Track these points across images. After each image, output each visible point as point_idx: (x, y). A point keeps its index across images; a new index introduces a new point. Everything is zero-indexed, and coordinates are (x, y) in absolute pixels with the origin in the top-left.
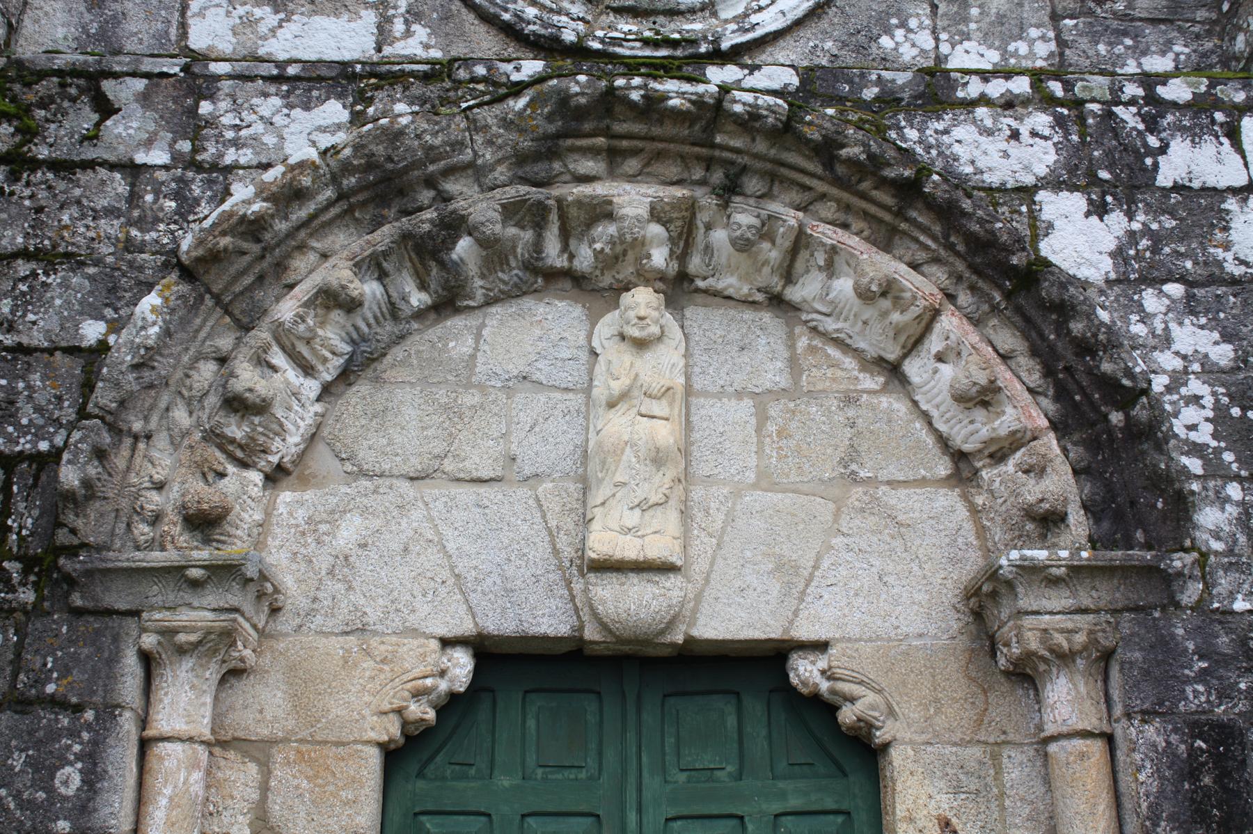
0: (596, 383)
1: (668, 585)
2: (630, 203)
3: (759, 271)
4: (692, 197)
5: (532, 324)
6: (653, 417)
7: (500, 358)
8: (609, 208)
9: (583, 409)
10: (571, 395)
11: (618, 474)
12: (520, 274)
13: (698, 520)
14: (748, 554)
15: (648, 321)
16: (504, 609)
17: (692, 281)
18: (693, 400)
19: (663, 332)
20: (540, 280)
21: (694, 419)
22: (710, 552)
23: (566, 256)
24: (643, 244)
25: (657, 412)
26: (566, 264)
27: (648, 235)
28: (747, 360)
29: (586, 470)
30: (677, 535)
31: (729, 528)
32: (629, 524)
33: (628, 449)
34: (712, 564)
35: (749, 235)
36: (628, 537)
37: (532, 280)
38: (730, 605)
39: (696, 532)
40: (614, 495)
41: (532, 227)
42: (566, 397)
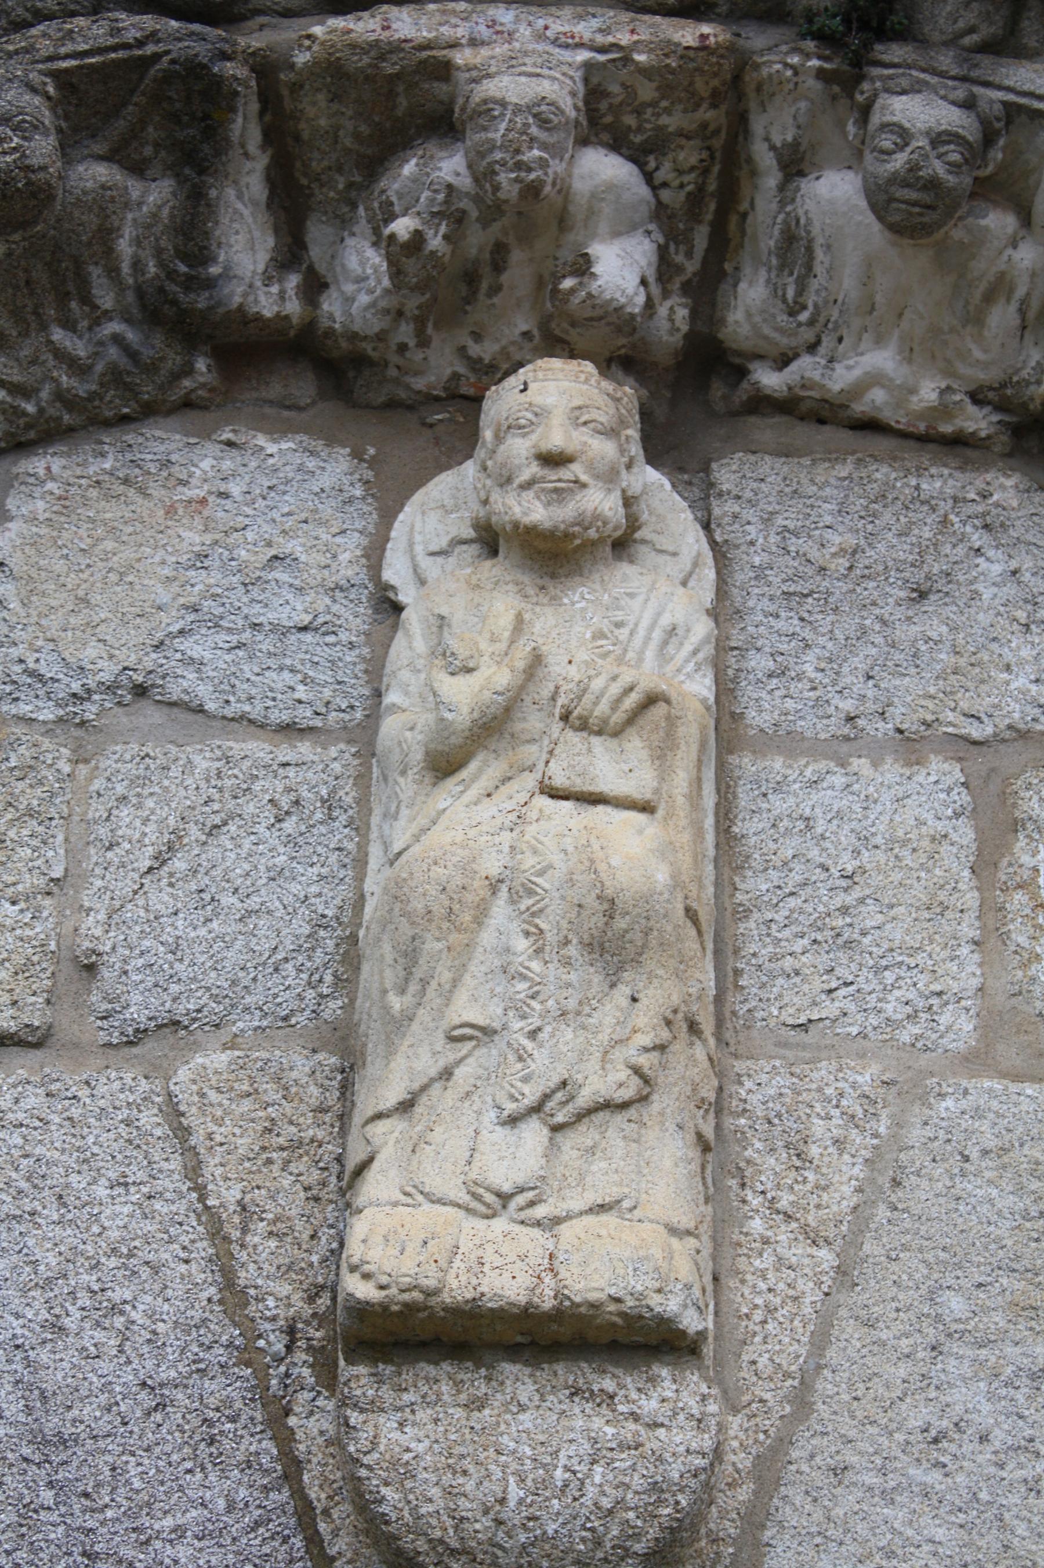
0: (391, 698)
1: (649, 1405)
2: (511, 63)
3: (976, 319)
4: (731, 48)
5: (170, 511)
6: (595, 799)
7: (53, 623)
8: (441, 89)
9: (348, 794)
10: (305, 749)
11: (462, 997)
12: (131, 335)
13: (767, 1180)
14: (955, 1304)
15: (576, 470)
16: (28, 1511)
17: (742, 372)
18: (745, 764)
19: (633, 524)
20: (201, 365)
21: (747, 826)
22: (812, 1296)
23: (293, 281)
24: (563, 221)
25: (609, 779)
26: (293, 307)
27: (580, 186)
28: (938, 629)
29: (349, 1007)
30: (686, 1222)
31: (882, 1212)
32: (503, 1178)
33: (500, 910)
34: (821, 1341)
35: (939, 168)
36: (500, 1224)
37: (174, 360)
38: (888, 1497)
39: (757, 1225)
40: (447, 1074)
41: (174, 170)
42: (285, 753)
